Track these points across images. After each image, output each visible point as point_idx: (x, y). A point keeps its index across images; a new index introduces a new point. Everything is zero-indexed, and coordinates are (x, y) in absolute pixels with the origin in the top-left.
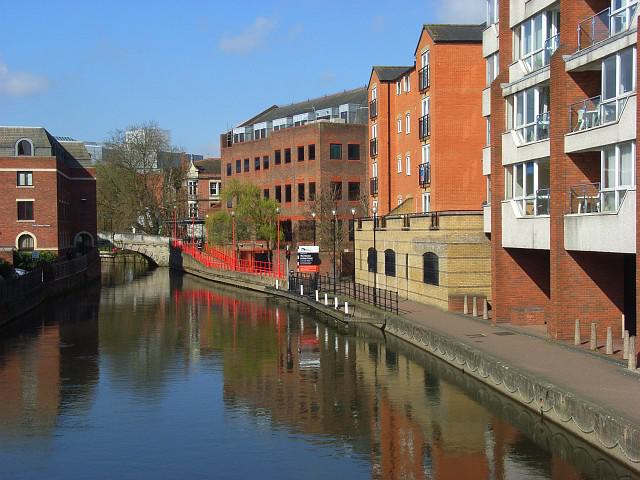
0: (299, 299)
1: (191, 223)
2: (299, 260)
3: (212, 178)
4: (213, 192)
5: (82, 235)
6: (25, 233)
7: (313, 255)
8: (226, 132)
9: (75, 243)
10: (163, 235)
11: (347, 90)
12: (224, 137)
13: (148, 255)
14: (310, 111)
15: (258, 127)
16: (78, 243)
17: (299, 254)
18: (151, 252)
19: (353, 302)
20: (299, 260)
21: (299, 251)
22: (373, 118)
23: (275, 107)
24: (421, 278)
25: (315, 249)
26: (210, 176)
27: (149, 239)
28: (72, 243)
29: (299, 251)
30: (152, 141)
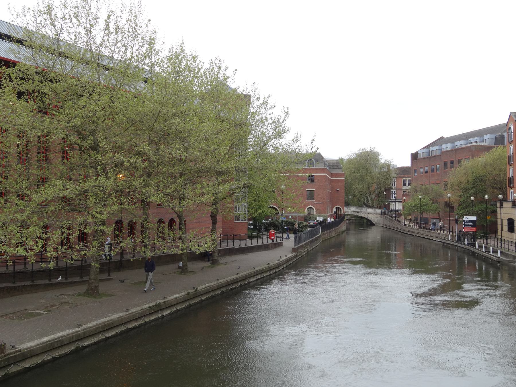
0: (464, 246)
1: (392, 202)
2: (464, 224)
3: (404, 177)
4: (405, 185)
5: (336, 208)
6: (310, 206)
7: (472, 221)
8: (413, 152)
9: (333, 212)
10: (377, 208)
11: (501, 123)
12: (412, 155)
13: (369, 219)
14: (466, 139)
15: (432, 149)
16: (334, 212)
17: (464, 221)
18: (371, 217)
19: (502, 250)
20: (464, 224)
21: (464, 219)
22: (110, 244)
23: (442, 138)
24: (507, 231)
25: (474, 218)
26: (403, 176)
27: (370, 210)
28: (332, 212)
29: (464, 219)
30: (378, 152)
